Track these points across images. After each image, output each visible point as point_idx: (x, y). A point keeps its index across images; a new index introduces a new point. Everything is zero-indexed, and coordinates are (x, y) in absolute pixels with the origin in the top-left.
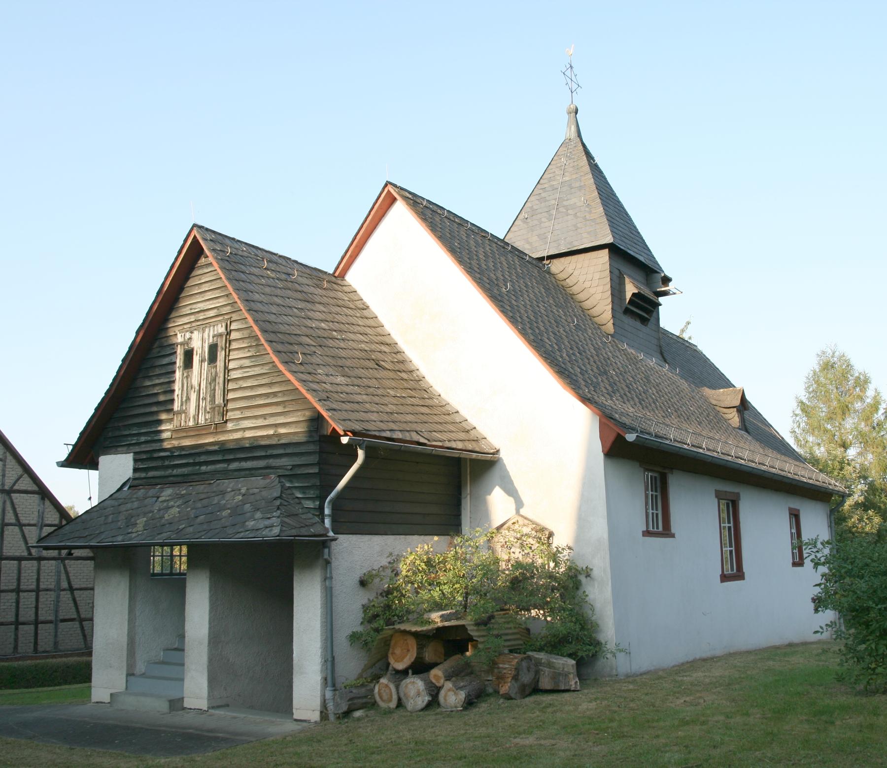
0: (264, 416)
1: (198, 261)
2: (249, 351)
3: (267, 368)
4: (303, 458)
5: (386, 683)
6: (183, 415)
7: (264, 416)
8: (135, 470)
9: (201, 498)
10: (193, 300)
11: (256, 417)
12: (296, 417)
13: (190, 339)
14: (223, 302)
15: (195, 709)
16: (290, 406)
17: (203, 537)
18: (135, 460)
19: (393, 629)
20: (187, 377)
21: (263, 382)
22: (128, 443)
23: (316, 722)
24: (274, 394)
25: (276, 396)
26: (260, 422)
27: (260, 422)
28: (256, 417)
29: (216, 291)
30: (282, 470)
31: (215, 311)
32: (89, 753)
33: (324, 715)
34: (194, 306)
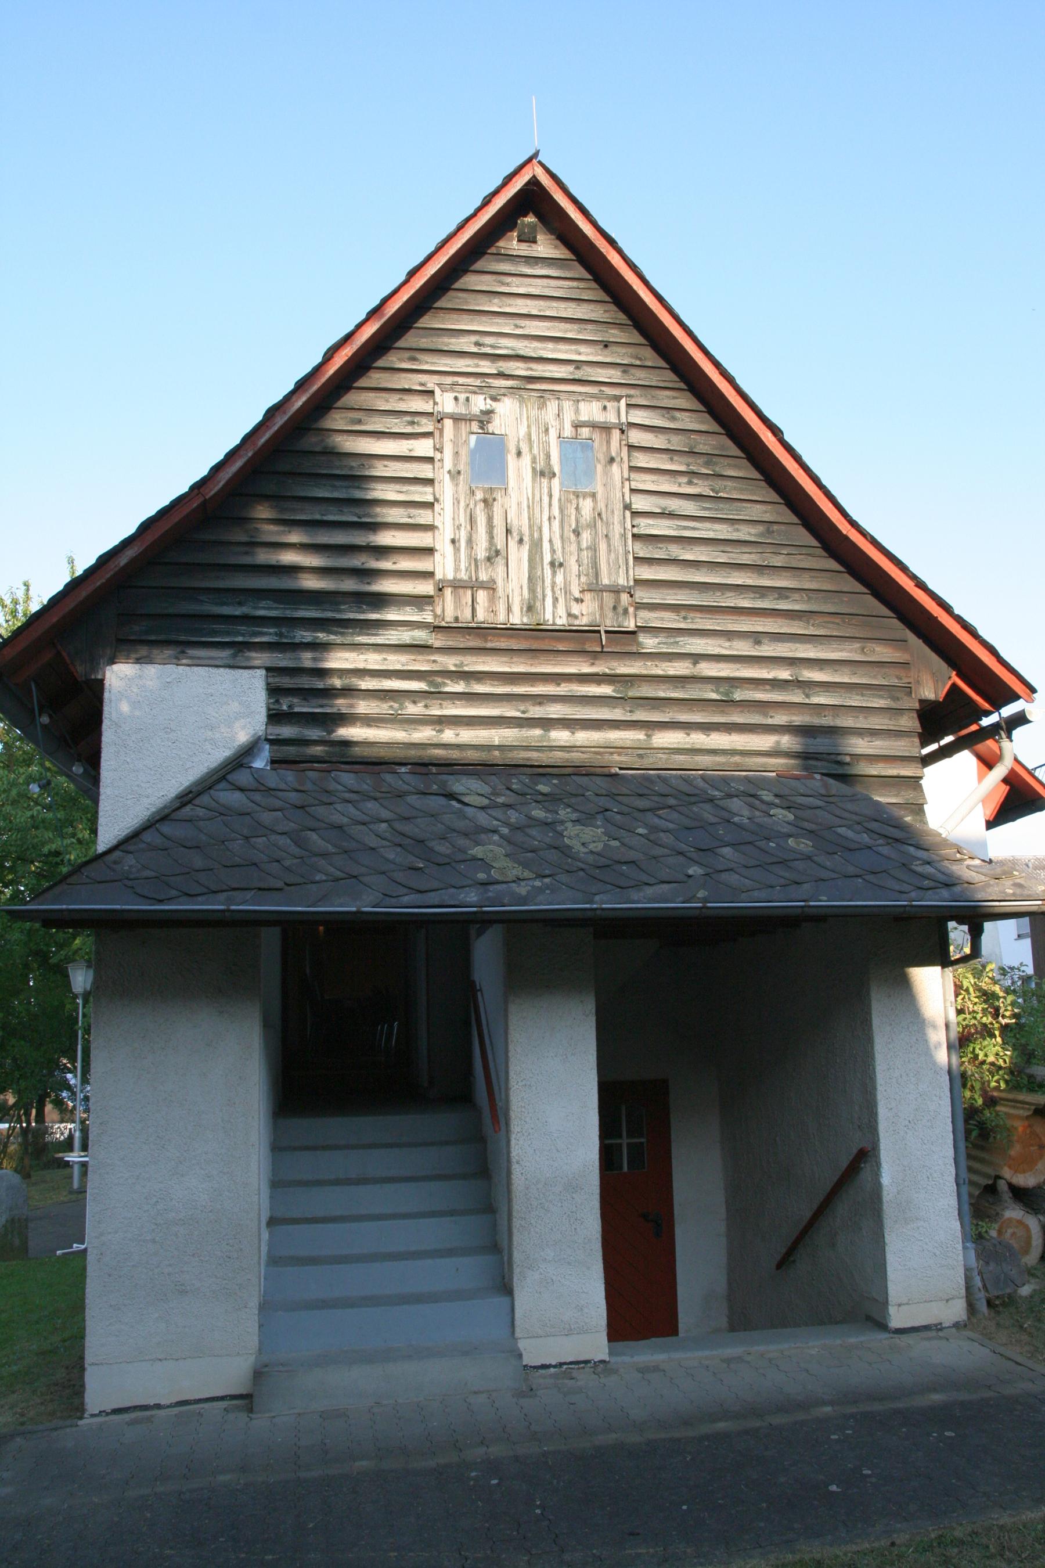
0: (757, 638)
1: (498, 239)
2: (690, 483)
3: (753, 531)
4: (878, 743)
5: (1019, 1217)
6: (482, 595)
7: (757, 638)
8: (275, 717)
9: (903, 889)
10: (480, 324)
11: (729, 635)
12: (850, 651)
13: (489, 413)
14: (588, 355)
15: (561, 1364)
16: (831, 626)
17: (541, 898)
18: (273, 691)
19: (86, 1002)
20: (487, 503)
21: (746, 559)
22: (240, 639)
23: (956, 1325)
24: (782, 593)
25: (787, 598)
26: (742, 648)
27: (742, 648)
28: (729, 635)
29: (568, 326)
30: (825, 764)
31: (571, 368)
32: (538, 1511)
33: (971, 1308)
34: (489, 340)
